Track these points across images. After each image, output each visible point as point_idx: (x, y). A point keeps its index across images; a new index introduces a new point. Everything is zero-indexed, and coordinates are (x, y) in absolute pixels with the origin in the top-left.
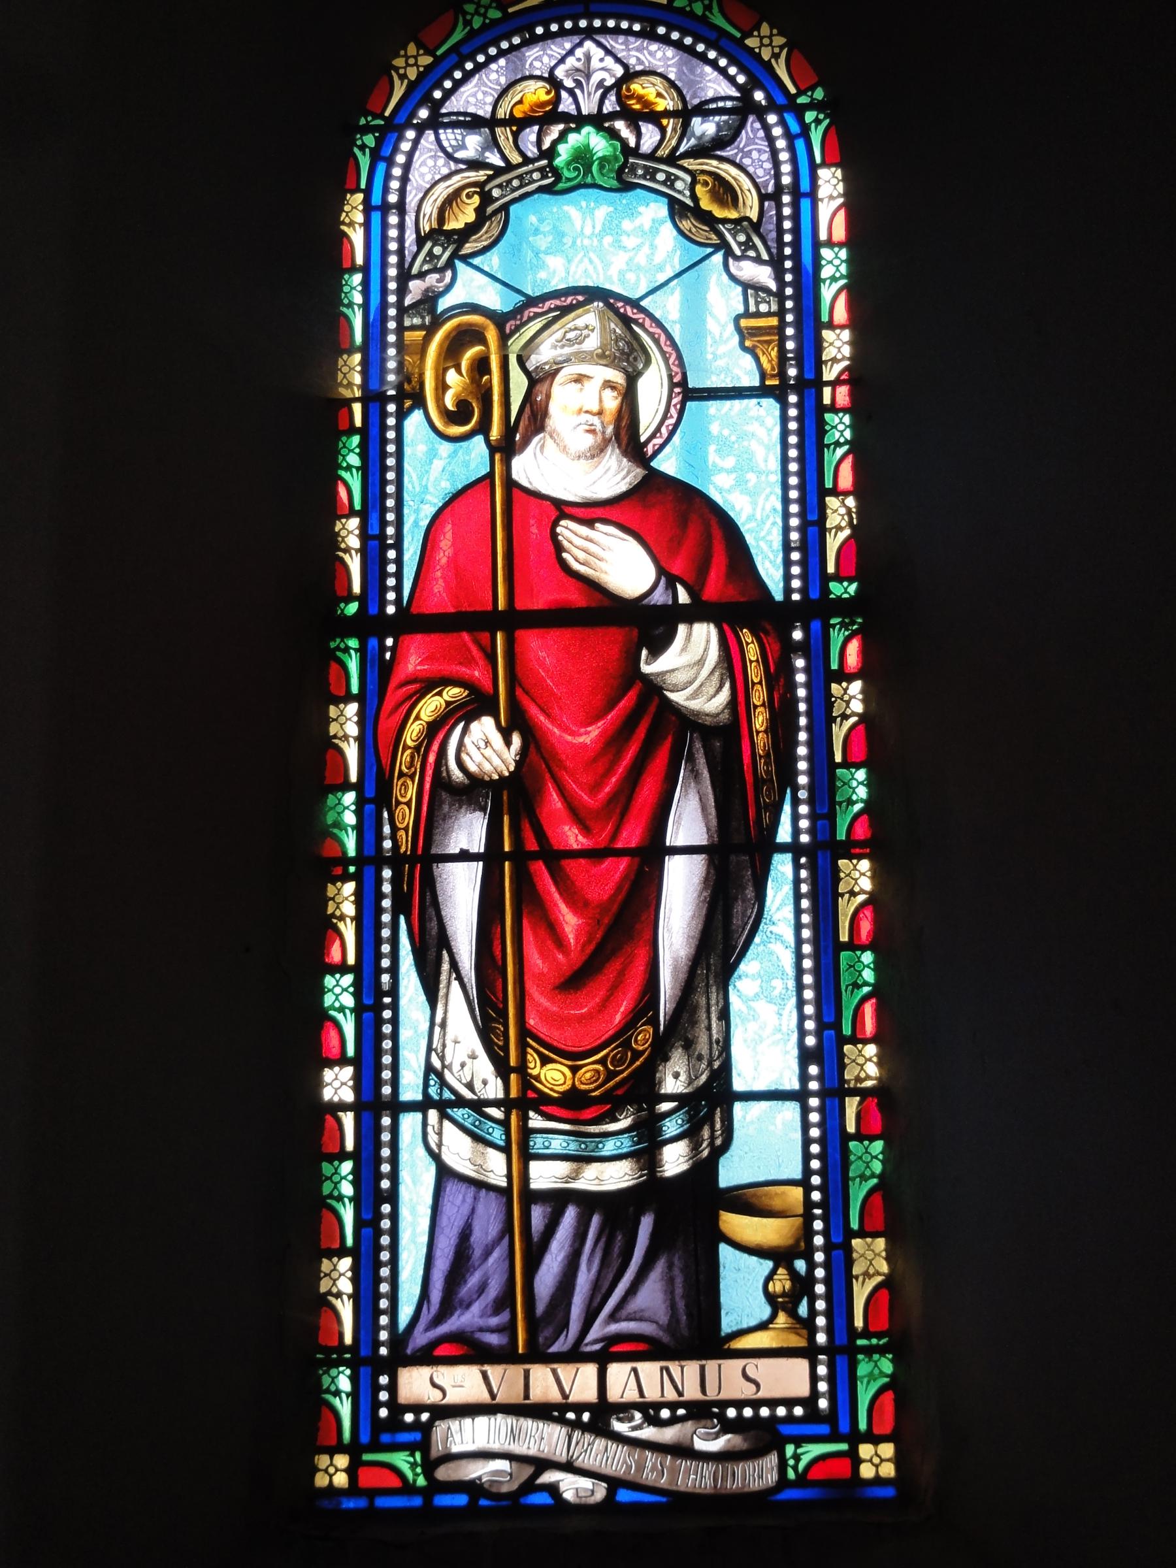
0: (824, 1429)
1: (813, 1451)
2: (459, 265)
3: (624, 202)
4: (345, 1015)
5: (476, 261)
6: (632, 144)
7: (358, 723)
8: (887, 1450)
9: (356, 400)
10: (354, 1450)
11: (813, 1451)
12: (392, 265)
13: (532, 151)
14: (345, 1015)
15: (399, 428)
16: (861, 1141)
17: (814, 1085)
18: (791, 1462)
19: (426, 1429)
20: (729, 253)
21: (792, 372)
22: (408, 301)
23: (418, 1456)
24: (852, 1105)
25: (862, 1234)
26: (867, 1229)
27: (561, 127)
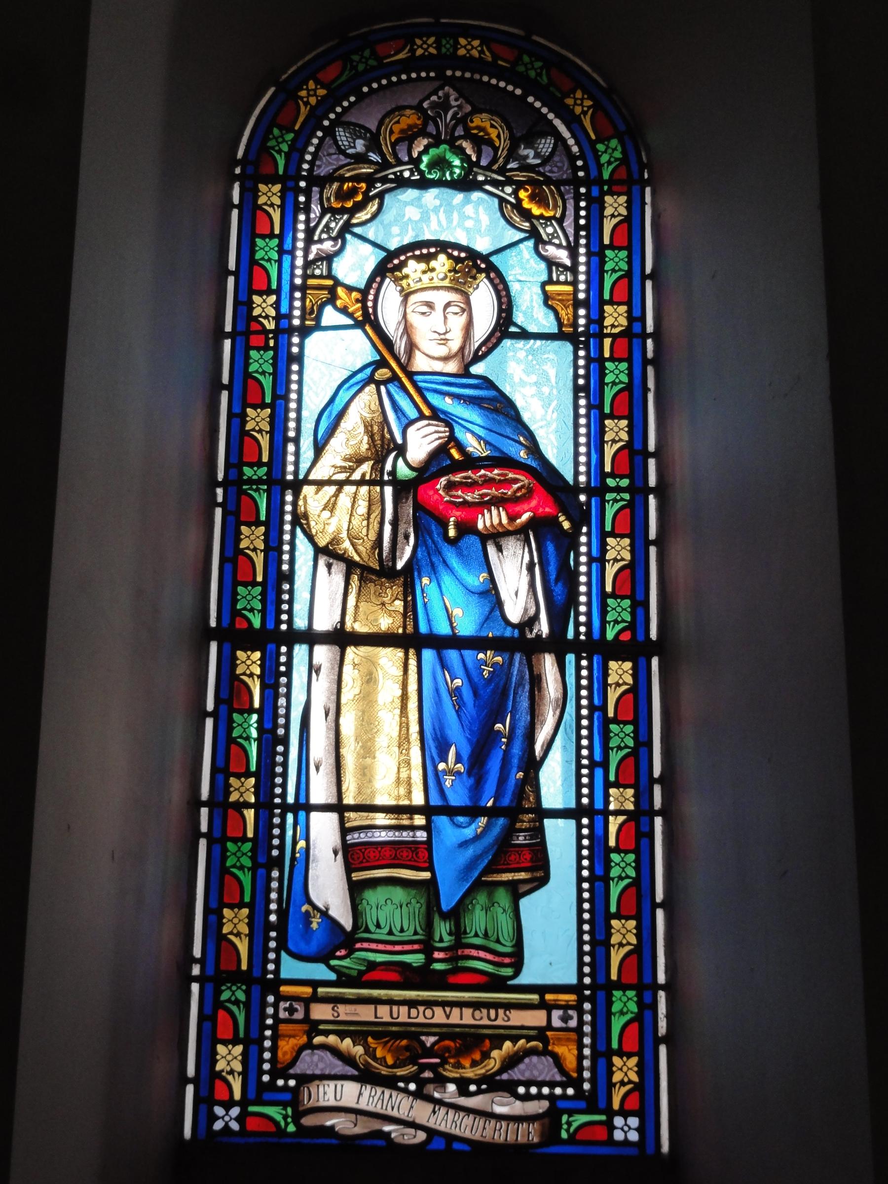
1: (581, 1119)
2: (348, 237)
4: (269, 321)
6: (474, 159)
7: (248, 924)
8: (634, 1122)
9: (248, 805)
11: (581, 1119)
14: (269, 321)
16: (620, 919)
17: (587, 980)
23: (289, 1110)
24: (607, 342)
26: (615, 414)
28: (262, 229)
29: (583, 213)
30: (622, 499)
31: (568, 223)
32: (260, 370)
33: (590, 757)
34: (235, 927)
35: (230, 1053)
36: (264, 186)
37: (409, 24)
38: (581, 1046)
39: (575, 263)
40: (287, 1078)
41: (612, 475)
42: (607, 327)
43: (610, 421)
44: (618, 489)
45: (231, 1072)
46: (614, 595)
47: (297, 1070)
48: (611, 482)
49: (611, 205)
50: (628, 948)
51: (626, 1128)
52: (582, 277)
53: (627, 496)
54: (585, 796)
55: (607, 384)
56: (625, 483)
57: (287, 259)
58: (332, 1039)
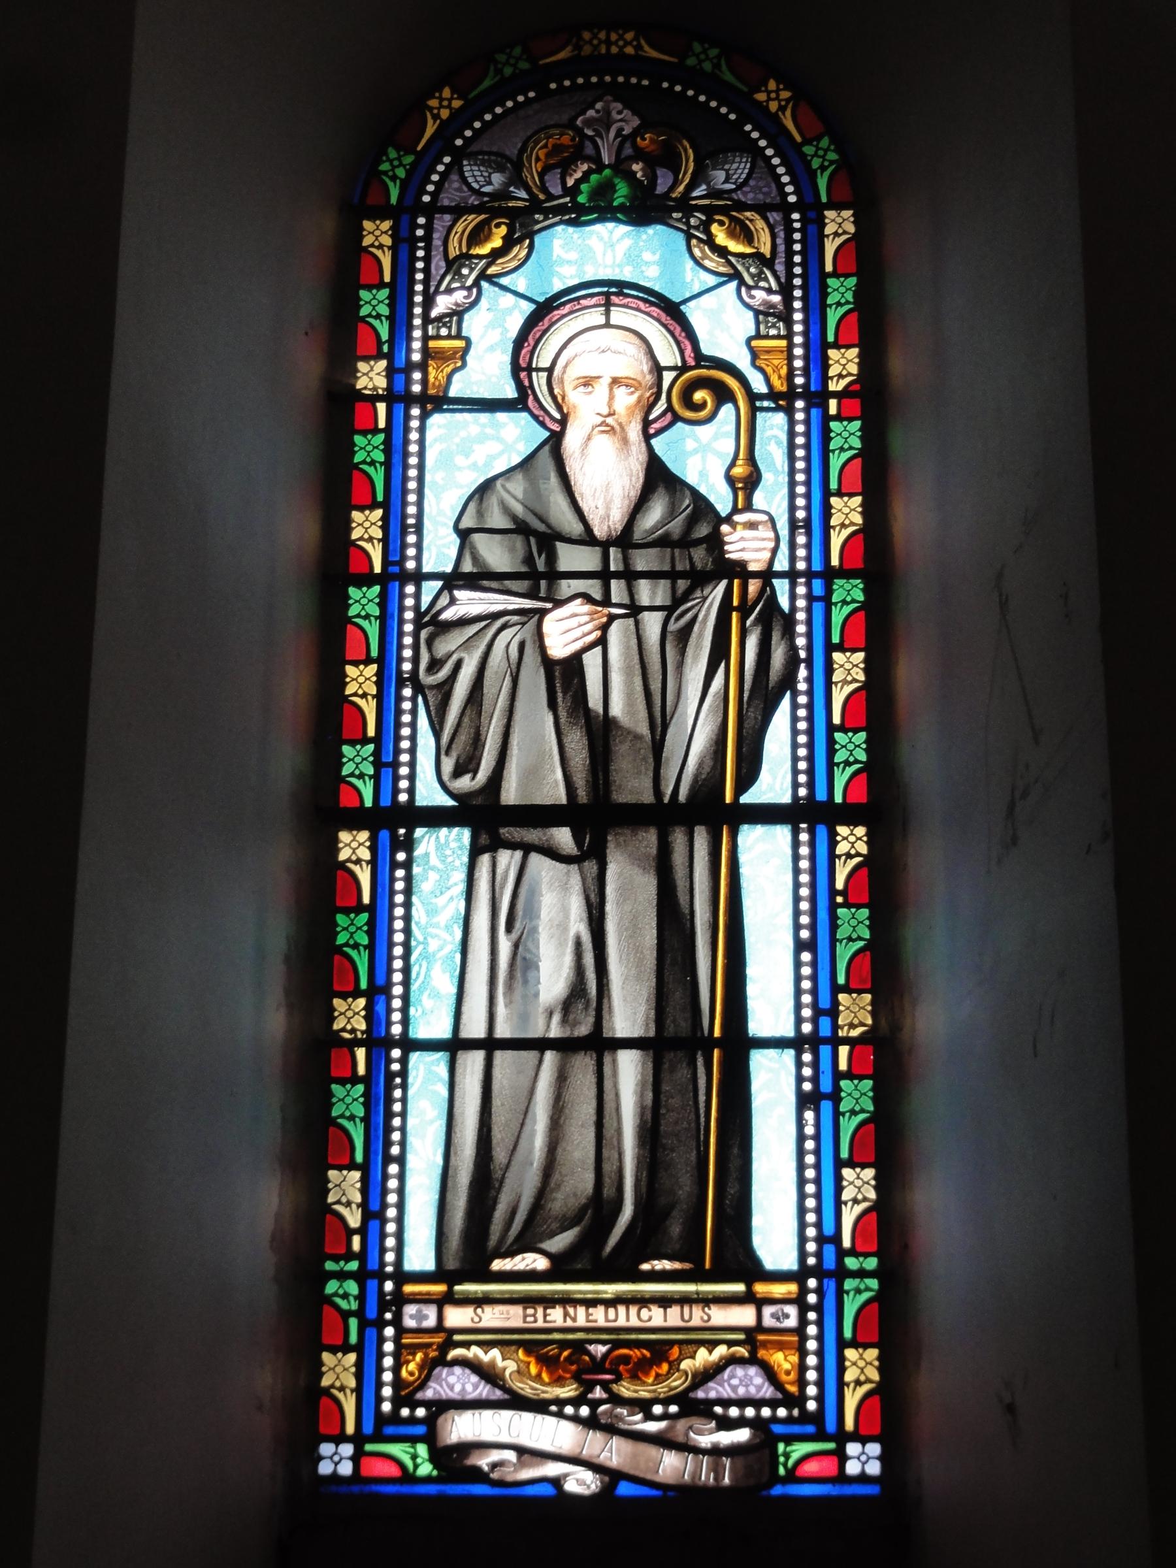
0: (810, 1429)
3: (644, 237)
5: (504, 281)
10: (358, 1440)
12: (417, 339)
13: (556, 190)
14: (364, 782)
15: (422, 430)
16: (853, 1168)
18: (782, 1459)
19: (431, 1422)
20: (742, 282)
21: (799, 381)
22: (434, 313)
24: (844, 1051)
25: (836, 345)
26: (856, 1160)
27: (585, 167)
28: (353, 650)
29: (797, 259)
30: (868, 1289)
31: (780, 268)
32: (368, 460)
33: (815, 1005)
34: (349, 1022)
35: (352, 924)
36: (331, 1355)
37: (556, 692)
38: (803, 1353)
39: (789, 309)
40: (413, 1406)
41: (853, 1252)
42: (842, 1028)
43: (848, 1082)
44: (861, 1274)
45: (358, 862)
46: (843, 728)
47: (429, 1394)
48: (851, 1263)
49: (838, 362)
50: (867, 1387)
51: (863, 1458)
52: (798, 328)
53: (873, 1283)
54: (797, 276)
55: (838, 765)
56: (871, 1263)
57: (387, 773)
58: (475, 1352)
